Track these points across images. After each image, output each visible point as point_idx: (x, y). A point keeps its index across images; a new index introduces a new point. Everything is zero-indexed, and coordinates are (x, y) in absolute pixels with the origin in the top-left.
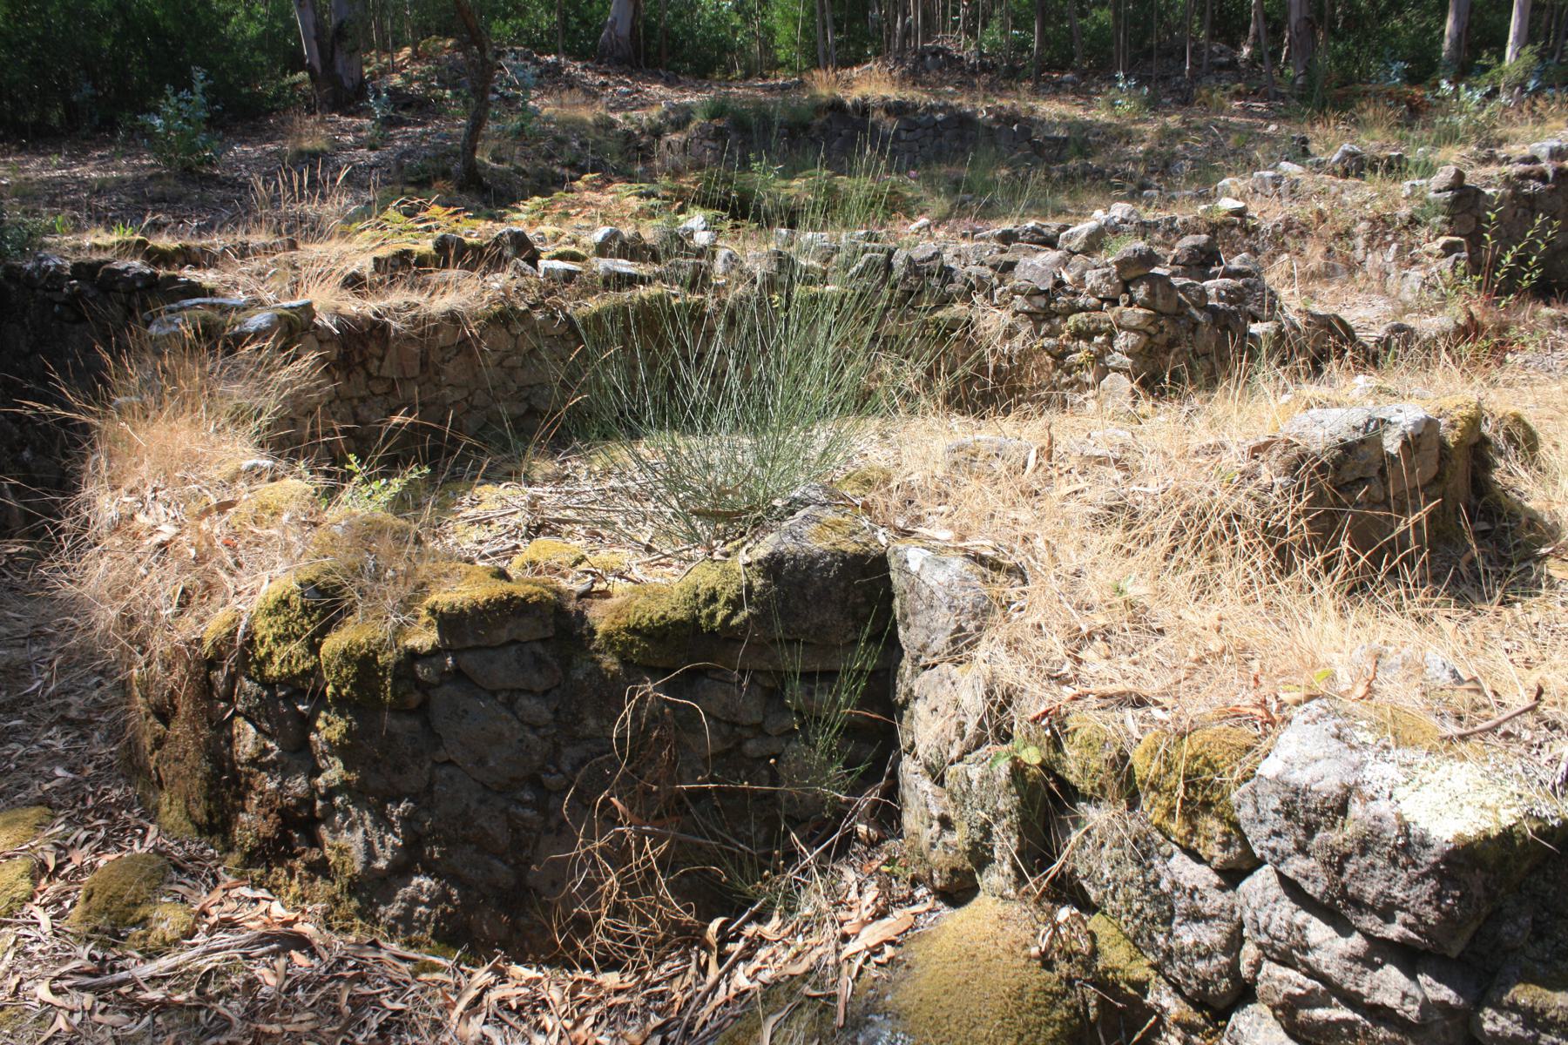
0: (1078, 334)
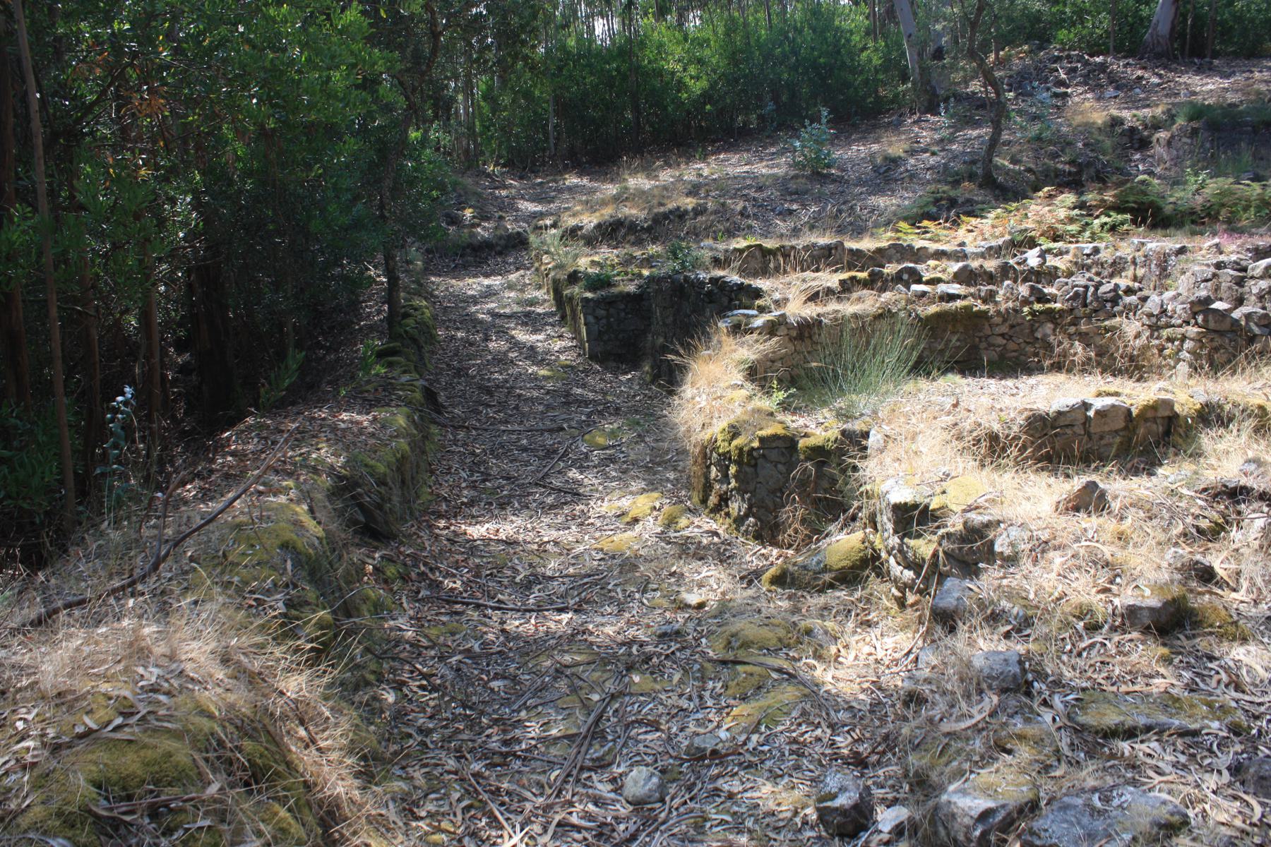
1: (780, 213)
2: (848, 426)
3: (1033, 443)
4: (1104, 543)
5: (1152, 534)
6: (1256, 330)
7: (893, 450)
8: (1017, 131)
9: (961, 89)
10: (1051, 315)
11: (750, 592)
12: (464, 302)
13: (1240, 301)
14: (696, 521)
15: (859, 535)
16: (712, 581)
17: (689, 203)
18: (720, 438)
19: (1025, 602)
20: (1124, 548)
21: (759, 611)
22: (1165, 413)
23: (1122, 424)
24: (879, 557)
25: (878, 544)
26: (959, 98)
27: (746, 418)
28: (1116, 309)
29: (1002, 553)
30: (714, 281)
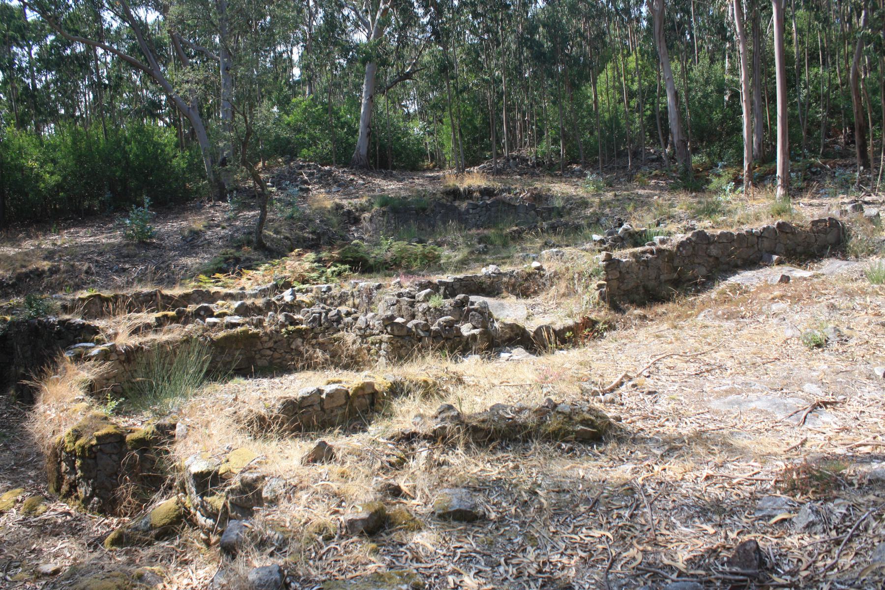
0: (372, 343)
1: (116, 271)
2: (161, 421)
3: (288, 420)
4: (333, 481)
5: (362, 471)
6: (422, 334)
7: (194, 436)
8: (277, 213)
9: (241, 185)
10: (300, 333)
11: (96, 554)
12: (374, 144)
13: (413, 317)
14: (52, 506)
15: (174, 499)
16: (66, 552)
17: (46, 265)
18: (67, 441)
19: (282, 529)
20: (346, 482)
21: (103, 568)
22: (368, 391)
23: (344, 401)
24: (189, 513)
25: (188, 504)
26: (239, 190)
27: (86, 423)
28: (340, 326)
29: (267, 498)
30: (62, 323)
